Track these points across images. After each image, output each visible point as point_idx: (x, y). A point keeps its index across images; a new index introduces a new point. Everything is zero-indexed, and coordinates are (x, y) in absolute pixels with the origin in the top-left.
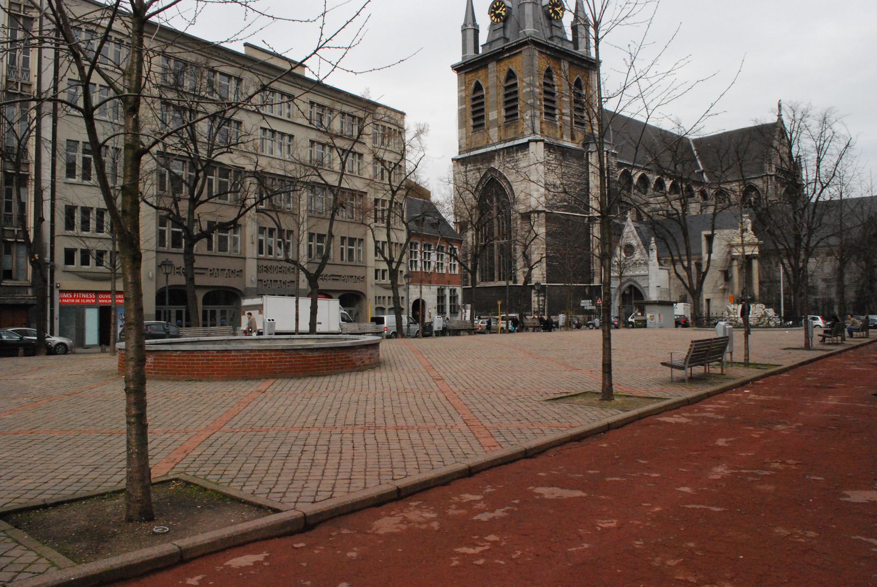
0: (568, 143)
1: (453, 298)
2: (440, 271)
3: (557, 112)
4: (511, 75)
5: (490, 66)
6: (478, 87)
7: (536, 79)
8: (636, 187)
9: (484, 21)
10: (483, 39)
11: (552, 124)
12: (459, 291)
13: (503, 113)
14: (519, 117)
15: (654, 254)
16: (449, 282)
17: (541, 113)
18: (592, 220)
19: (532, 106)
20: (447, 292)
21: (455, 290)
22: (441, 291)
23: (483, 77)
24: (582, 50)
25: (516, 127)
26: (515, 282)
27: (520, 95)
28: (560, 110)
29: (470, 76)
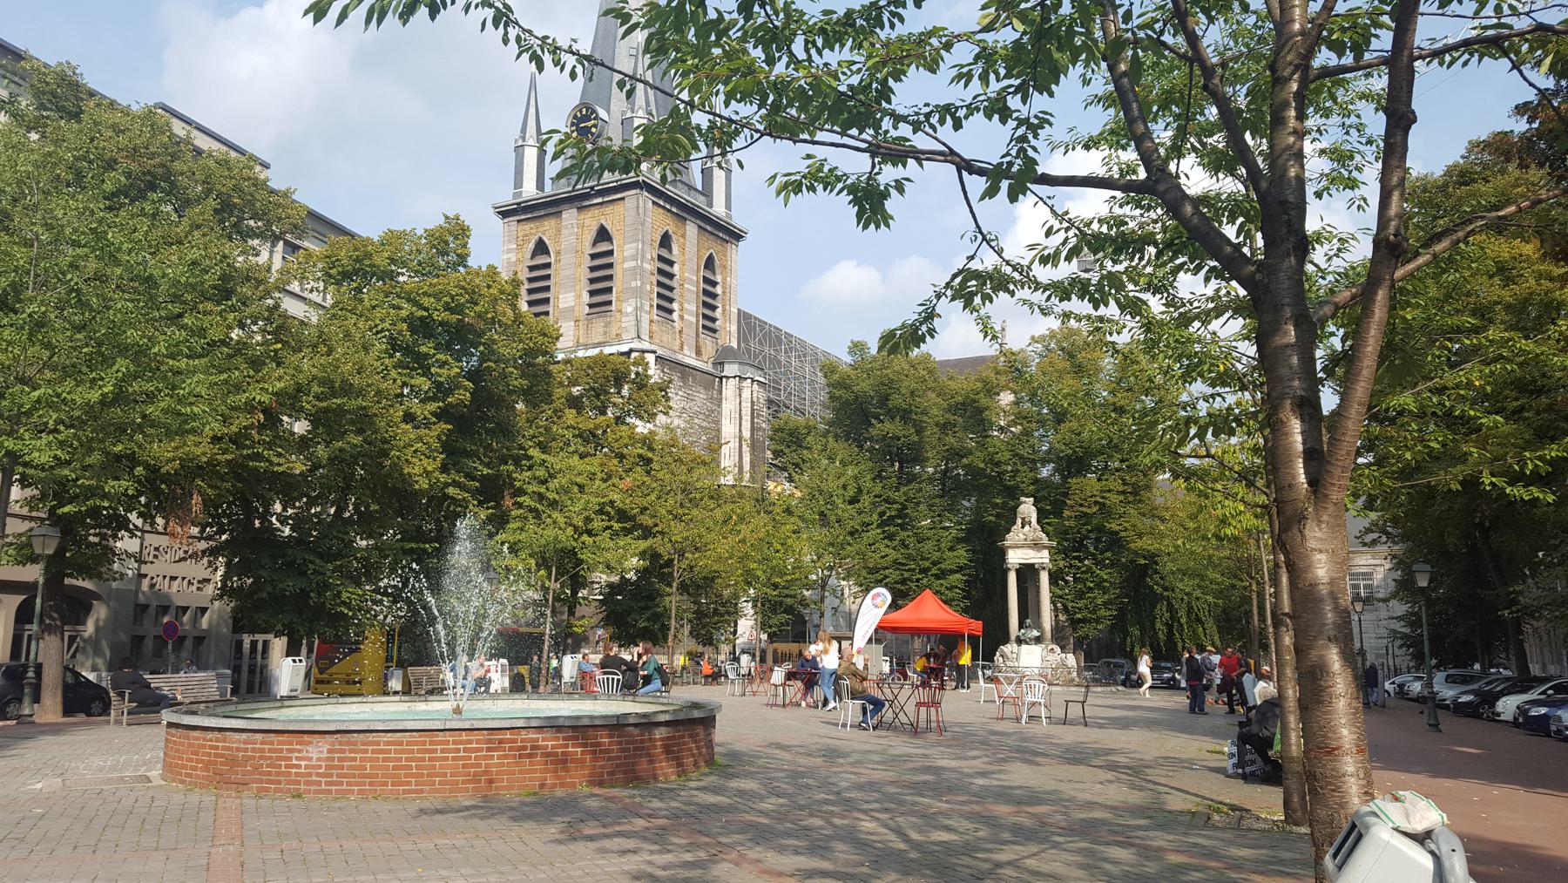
4: (603, 235)
14: (613, 307)
19: (638, 293)
23: (552, 233)
25: (607, 325)
28: (681, 305)
29: (527, 227)
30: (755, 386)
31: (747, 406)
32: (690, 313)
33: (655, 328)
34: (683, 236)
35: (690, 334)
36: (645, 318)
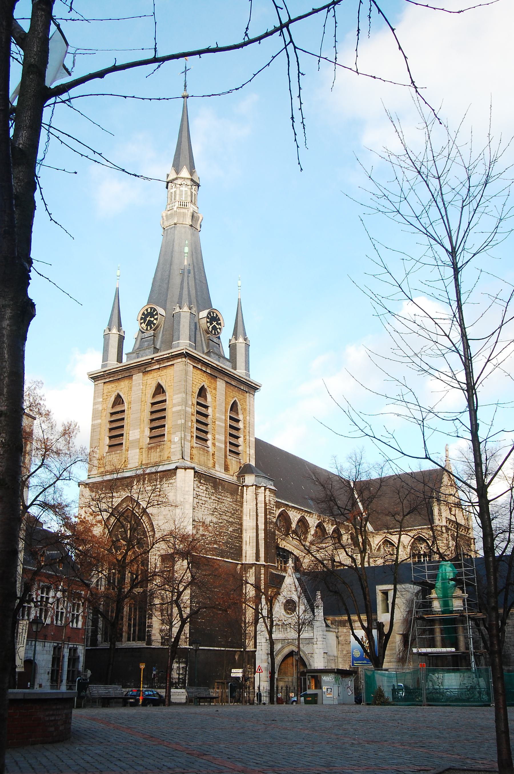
0: (219, 473)
1: (73, 660)
2: (75, 625)
3: (209, 436)
4: (159, 389)
5: (134, 377)
6: (118, 400)
7: (189, 397)
8: (294, 532)
9: (132, 328)
10: (128, 346)
11: (205, 449)
12: (81, 651)
13: (147, 432)
15: (320, 613)
16: (69, 639)
17: (192, 436)
18: (246, 567)
20: (66, 652)
21: (75, 649)
22: (58, 650)
23: (126, 389)
24: (240, 372)
26: (149, 642)
27: (169, 414)
28: (214, 435)
29: (110, 386)
30: (267, 492)
31: (261, 506)
32: (220, 441)
33: (195, 451)
34: (215, 389)
35: (220, 457)
36: (188, 446)
